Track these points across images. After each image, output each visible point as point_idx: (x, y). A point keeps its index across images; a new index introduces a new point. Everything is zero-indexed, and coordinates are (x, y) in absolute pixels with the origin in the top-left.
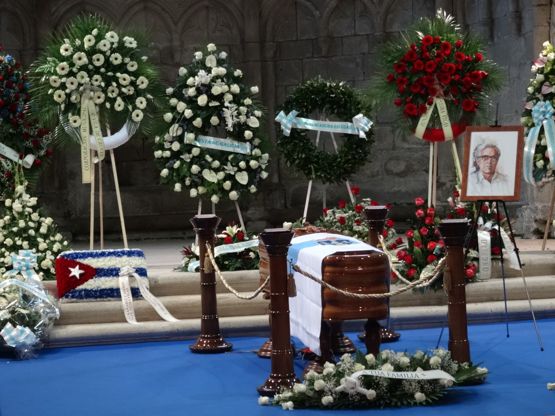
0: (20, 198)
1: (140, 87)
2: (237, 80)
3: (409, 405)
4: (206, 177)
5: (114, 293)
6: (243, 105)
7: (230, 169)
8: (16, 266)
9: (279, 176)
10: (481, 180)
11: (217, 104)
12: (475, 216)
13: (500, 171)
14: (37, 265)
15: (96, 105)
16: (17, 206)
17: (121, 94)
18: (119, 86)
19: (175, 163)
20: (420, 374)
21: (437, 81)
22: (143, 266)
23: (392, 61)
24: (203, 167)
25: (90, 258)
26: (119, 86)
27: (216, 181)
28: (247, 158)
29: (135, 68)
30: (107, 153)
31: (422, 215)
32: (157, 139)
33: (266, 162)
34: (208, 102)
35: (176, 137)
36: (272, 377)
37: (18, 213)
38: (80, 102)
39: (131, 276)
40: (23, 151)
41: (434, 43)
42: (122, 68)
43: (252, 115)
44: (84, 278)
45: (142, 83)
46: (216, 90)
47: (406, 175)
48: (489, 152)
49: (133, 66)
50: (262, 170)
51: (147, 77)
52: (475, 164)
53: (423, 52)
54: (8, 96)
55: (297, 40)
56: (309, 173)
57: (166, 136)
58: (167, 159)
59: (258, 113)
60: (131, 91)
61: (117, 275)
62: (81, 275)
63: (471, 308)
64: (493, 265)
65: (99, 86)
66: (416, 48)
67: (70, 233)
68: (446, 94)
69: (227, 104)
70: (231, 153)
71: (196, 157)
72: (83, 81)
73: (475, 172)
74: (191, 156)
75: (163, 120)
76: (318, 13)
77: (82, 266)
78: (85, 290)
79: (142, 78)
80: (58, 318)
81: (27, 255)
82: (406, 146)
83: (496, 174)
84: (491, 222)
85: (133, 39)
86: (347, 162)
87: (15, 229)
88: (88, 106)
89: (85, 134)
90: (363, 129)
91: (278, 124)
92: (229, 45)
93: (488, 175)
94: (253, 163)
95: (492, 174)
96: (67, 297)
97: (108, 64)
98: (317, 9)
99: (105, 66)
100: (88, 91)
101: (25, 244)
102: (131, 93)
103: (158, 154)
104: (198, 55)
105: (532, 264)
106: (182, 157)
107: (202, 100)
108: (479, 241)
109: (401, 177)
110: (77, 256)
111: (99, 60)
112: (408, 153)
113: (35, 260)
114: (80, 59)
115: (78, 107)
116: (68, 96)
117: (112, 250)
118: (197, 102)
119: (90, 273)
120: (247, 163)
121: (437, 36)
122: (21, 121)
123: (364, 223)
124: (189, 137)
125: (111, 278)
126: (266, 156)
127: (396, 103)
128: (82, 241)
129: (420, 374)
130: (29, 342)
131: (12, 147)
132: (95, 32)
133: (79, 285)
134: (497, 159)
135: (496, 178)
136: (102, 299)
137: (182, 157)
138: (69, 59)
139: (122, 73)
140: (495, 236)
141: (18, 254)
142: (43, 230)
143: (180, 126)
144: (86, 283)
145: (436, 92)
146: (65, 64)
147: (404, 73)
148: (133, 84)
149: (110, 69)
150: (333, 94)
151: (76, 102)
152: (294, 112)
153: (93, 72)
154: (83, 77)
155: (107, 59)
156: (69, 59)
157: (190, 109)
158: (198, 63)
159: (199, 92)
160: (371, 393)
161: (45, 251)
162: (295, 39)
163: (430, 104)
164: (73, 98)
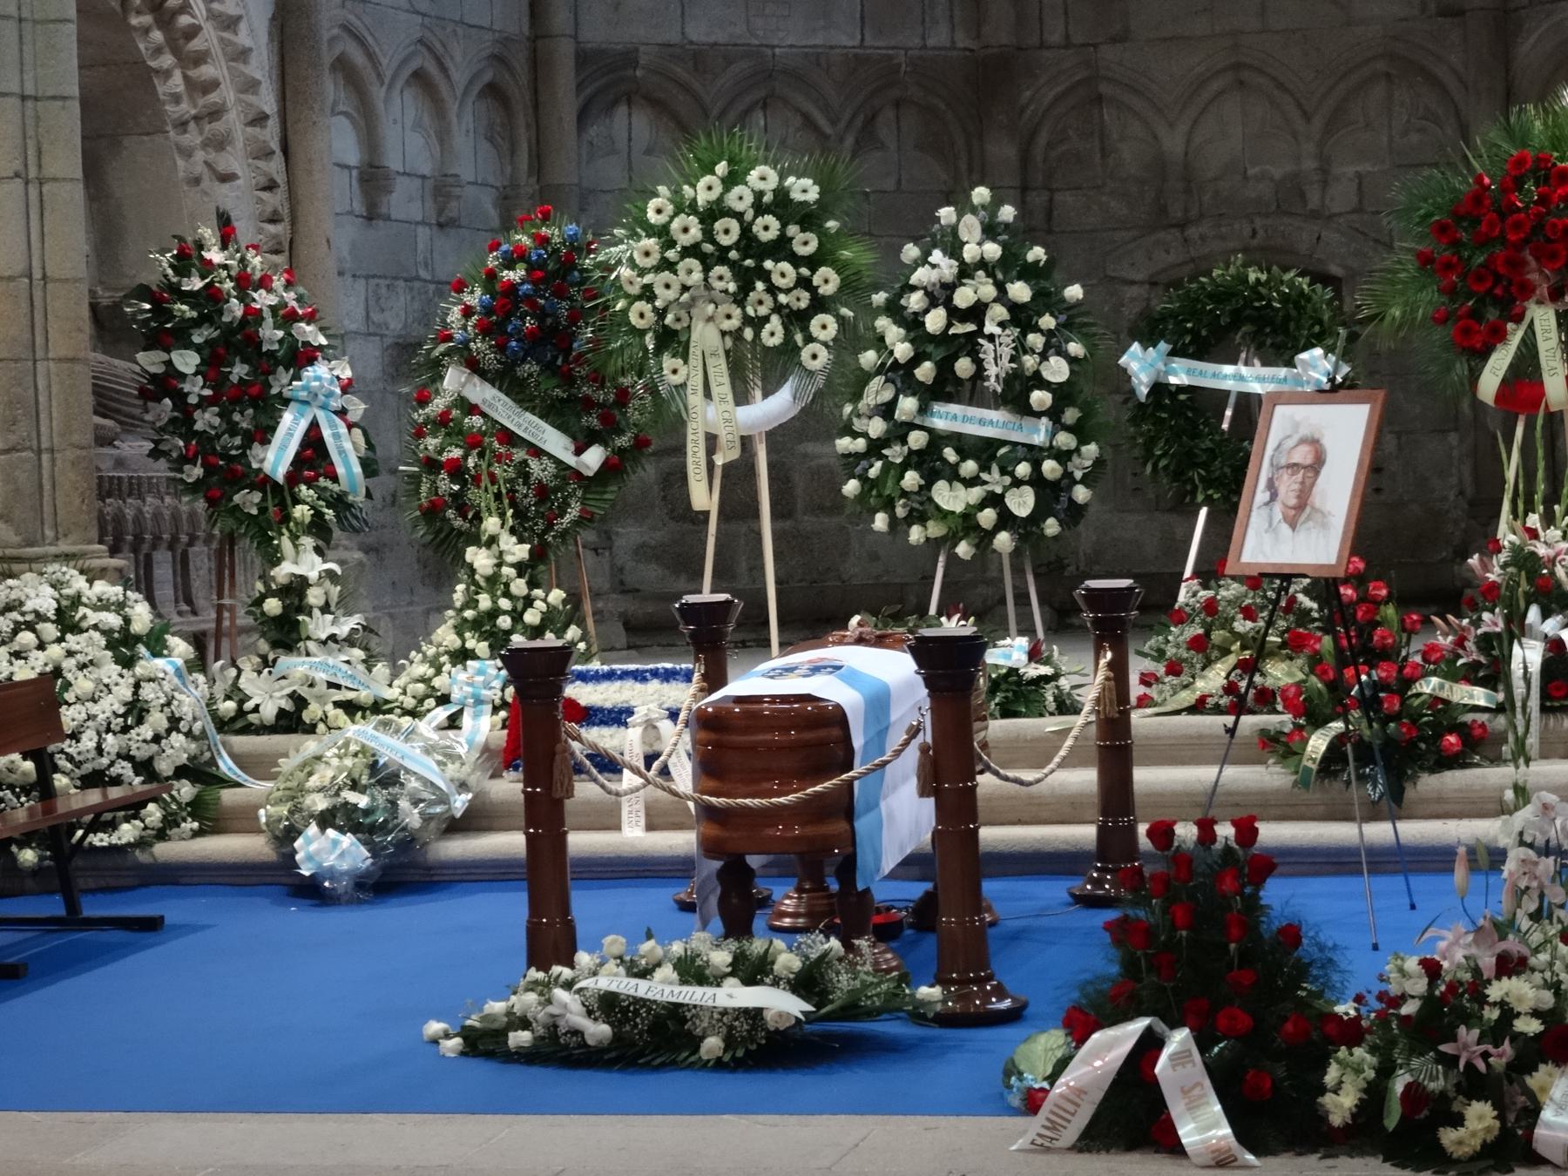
0: (494, 547)
1: (821, 291)
2: (1029, 273)
3: (672, 1065)
4: (938, 499)
10: (1275, 522)
11: (971, 327)
13: (1318, 504)
15: (724, 334)
17: (778, 308)
18: (772, 290)
19: (872, 466)
20: (736, 995)
21: (1533, 263)
23: (1429, 215)
24: (930, 479)
26: (772, 290)
28: (1034, 454)
29: (812, 247)
30: (746, 442)
32: (848, 409)
33: (1088, 463)
34: (949, 325)
35: (877, 406)
37: (488, 579)
39: (650, 725)
42: (781, 249)
45: (826, 281)
46: (964, 297)
48: (1303, 455)
49: (806, 243)
50: (1076, 482)
52: (1271, 485)
53: (1504, 189)
56: (1194, 493)
58: (856, 457)
59: (1075, 348)
60: (803, 300)
63: (991, 835)
65: (726, 291)
66: (1487, 180)
69: (990, 328)
70: (1004, 443)
71: (919, 453)
73: (1267, 504)
79: (824, 271)
81: (480, 672)
83: (1308, 510)
85: (810, 182)
87: (469, 614)
88: (705, 337)
89: (695, 399)
91: (1124, 375)
94: (1050, 467)
95: (1300, 511)
97: (748, 240)
100: (700, 303)
101: (482, 648)
102: (803, 304)
104: (946, 214)
107: (935, 321)
111: (728, 233)
114: (686, 230)
115: (684, 339)
116: (661, 314)
117: (632, 667)
120: (1036, 466)
121: (1547, 151)
124: (908, 406)
125: (613, 730)
126: (1091, 450)
127: (1434, 319)
129: (736, 995)
132: (722, 168)
135: (1309, 518)
138: (662, 232)
139: (777, 261)
141: (465, 669)
146: (651, 243)
147: (1456, 243)
148: (804, 283)
151: (678, 327)
152: (1163, 346)
153: (714, 260)
154: (690, 272)
155: (746, 230)
156: (662, 232)
159: (933, 302)
160: (598, 1031)
163: (1518, 319)
164: (669, 319)
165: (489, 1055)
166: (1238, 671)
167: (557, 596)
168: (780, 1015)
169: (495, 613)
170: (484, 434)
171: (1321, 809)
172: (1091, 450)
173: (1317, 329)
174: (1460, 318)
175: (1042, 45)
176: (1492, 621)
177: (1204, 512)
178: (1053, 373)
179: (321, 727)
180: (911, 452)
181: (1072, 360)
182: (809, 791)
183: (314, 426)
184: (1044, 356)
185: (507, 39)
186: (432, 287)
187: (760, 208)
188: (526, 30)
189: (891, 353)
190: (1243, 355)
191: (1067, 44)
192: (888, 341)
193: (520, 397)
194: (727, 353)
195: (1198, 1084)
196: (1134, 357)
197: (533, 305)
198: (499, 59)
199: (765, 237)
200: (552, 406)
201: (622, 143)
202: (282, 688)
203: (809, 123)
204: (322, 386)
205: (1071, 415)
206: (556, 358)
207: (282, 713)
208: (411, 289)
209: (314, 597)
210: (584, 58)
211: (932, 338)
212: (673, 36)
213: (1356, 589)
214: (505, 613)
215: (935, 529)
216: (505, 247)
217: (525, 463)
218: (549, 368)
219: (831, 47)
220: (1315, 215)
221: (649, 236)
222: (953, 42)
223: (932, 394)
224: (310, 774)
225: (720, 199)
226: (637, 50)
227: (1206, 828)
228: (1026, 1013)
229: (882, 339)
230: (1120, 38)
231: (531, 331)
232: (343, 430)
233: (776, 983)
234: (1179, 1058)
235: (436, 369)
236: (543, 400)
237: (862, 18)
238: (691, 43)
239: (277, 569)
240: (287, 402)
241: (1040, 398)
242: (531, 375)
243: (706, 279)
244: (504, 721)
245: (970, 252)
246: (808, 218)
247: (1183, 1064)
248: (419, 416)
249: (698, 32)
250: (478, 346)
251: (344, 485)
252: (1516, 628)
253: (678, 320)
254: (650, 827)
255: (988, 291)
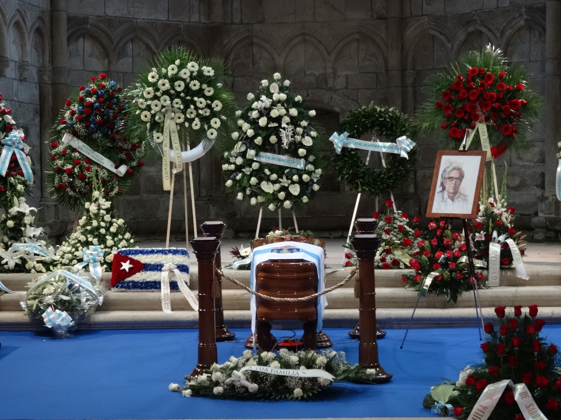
0: (97, 203)
1: (215, 109)
2: (296, 105)
3: (286, 399)
4: (263, 188)
5: (155, 285)
6: (300, 126)
7: (285, 182)
8: (85, 259)
9: (416, 187)
10: (445, 198)
11: (276, 125)
12: (490, 229)
13: (462, 192)
14: (103, 258)
15: (177, 124)
16: (93, 208)
17: (198, 115)
18: (197, 108)
19: (237, 175)
20: (304, 372)
21: (479, 108)
22: (185, 264)
23: (440, 89)
24: (260, 180)
25: (140, 254)
26: (197, 108)
27: (271, 192)
28: (300, 173)
31: (433, 228)
32: (226, 154)
33: (318, 176)
34: (268, 123)
35: (239, 153)
36: (199, 367)
37: (95, 215)
38: (164, 121)
39: (171, 271)
40: (118, 163)
41: (479, 74)
42: (200, 93)
43: (307, 135)
44: (132, 271)
45: (217, 106)
46: (274, 113)
47: (521, 189)
48: (455, 174)
49: (209, 91)
50: (314, 183)
51: (222, 102)
52: (442, 184)
53: (468, 81)
54: (108, 116)
55: (433, 69)
56: (357, 188)
57: (233, 152)
58: (231, 172)
60: (208, 113)
61: (161, 270)
62: (130, 269)
63: (381, 313)
64: (501, 275)
65: (179, 108)
66: (462, 78)
67: (232, 230)
68: (487, 120)
69: (284, 125)
70: (287, 168)
71: (256, 170)
72: (165, 104)
73: (441, 192)
74: (251, 169)
75: (231, 138)
76: (450, 45)
77: (132, 261)
78: (133, 282)
79: (216, 102)
80: (101, 304)
81: (95, 250)
82: (521, 163)
83: (458, 194)
84: (504, 235)
85: (211, 68)
86: (390, 178)
87: (89, 228)
88: (170, 125)
89: (166, 148)
90: (405, 150)
91: (332, 143)
92: (376, 73)
93: (452, 195)
94: (305, 177)
95: (455, 194)
96: (117, 287)
98: (449, 41)
99: (185, 91)
100: (169, 112)
101: (95, 241)
102: (208, 114)
103: (225, 167)
104: (265, 82)
105: (539, 274)
106: (243, 170)
107: (263, 122)
108: (490, 252)
109: (515, 190)
110: (130, 252)
111: (180, 86)
112: (522, 170)
113: (102, 254)
114: (164, 85)
115: (161, 126)
116: (153, 116)
118: (258, 123)
119: (138, 267)
120: (300, 177)
122: (118, 137)
123: (392, 233)
124: (251, 153)
125: (155, 272)
126: (319, 171)
127: (442, 127)
128: (243, 237)
129: (304, 372)
130: (64, 324)
131: (109, 158)
132: (178, 62)
133: (128, 277)
134: (461, 181)
135: (458, 197)
136: (147, 290)
137: (243, 170)
138: (154, 85)
139: (199, 97)
140: (505, 248)
141: (88, 249)
142: (113, 229)
143: (243, 143)
144: (134, 276)
145: (478, 118)
146: (150, 89)
147: (450, 100)
148: (209, 106)
149: (189, 94)
150: (382, 118)
151: (160, 121)
152: (346, 134)
154: (165, 101)
157: (253, 129)
158: (263, 89)
159: (261, 114)
160: (253, 387)
161: (111, 248)
162: (432, 67)
163: (473, 128)
164: (157, 118)
165: (205, 396)
166: (385, 253)
167: (121, 221)
168: (325, 380)
169: (98, 228)
170: (80, 159)
171: (425, 304)
172: (319, 171)
173: (404, 129)
174: (452, 127)
175: (232, 23)
176: (480, 236)
177: (359, 195)
178: (307, 142)
179: (33, 270)
180: (253, 170)
181: (313, 138)
182: (313, 295)
183: (14, 155)
184: (303, 136)
185: (43, 11)
186: (18, 103)
187: (192, 78)
188: (49, 8)
189: (246, 133)
190: (373, 138)
191: (242, 23)
192: (244, 129)
193: (93, 146)
194: (178, 131)
195: (532, 404)
196: (335, 138)
197: (100, 111)
198: (40, 18)
199: (194, 88)
200: (106, 150)
201: (81, 53)
202: (16, 255)
203: (148, 47)
204: (17, 140)
205: (312, 158)
206: (108, 132)
207: (17, 265)
208: (11, 104)
209: (28, 220)
210: (70, 20)
211: (261, 128)
212: (102, 14)
213: (436, 224)
214: (103, 227)
215: (261, 199)
216: (87, 89)
217: (97, 171)
218: (105, 135)
219: (157, 20)
220: (331, 89)
221: (149, 87)
222: (200, 20)
223: (260, 149)
224: (44, 288)
225: (177, 73)
226: (88, 18)
227: (518, 309)
228: (391, 379)
229: (240, 128)
230: (262, 22)
231: (100, 121)
232: (24, 156)
233: (319, 368)
234: (522, 395)
235: (59, 134)
236: (103, 147)
237: (168, 10)
238: (108, 16)
239: (12, 209)
240: (3, 145)
241: (302, 152)
242: (98, 138)
243: (171, 104)
244: (106, 269)
245: (276, 97)
246: (210, 82)
247: (525, 397)
248: (53, 152)
249: (110, 12)
250: (78, 126)
251: (26, 178)
252: (489, 239)
253: (160, 118)
254: (173, 310)
255: (283, 111)
